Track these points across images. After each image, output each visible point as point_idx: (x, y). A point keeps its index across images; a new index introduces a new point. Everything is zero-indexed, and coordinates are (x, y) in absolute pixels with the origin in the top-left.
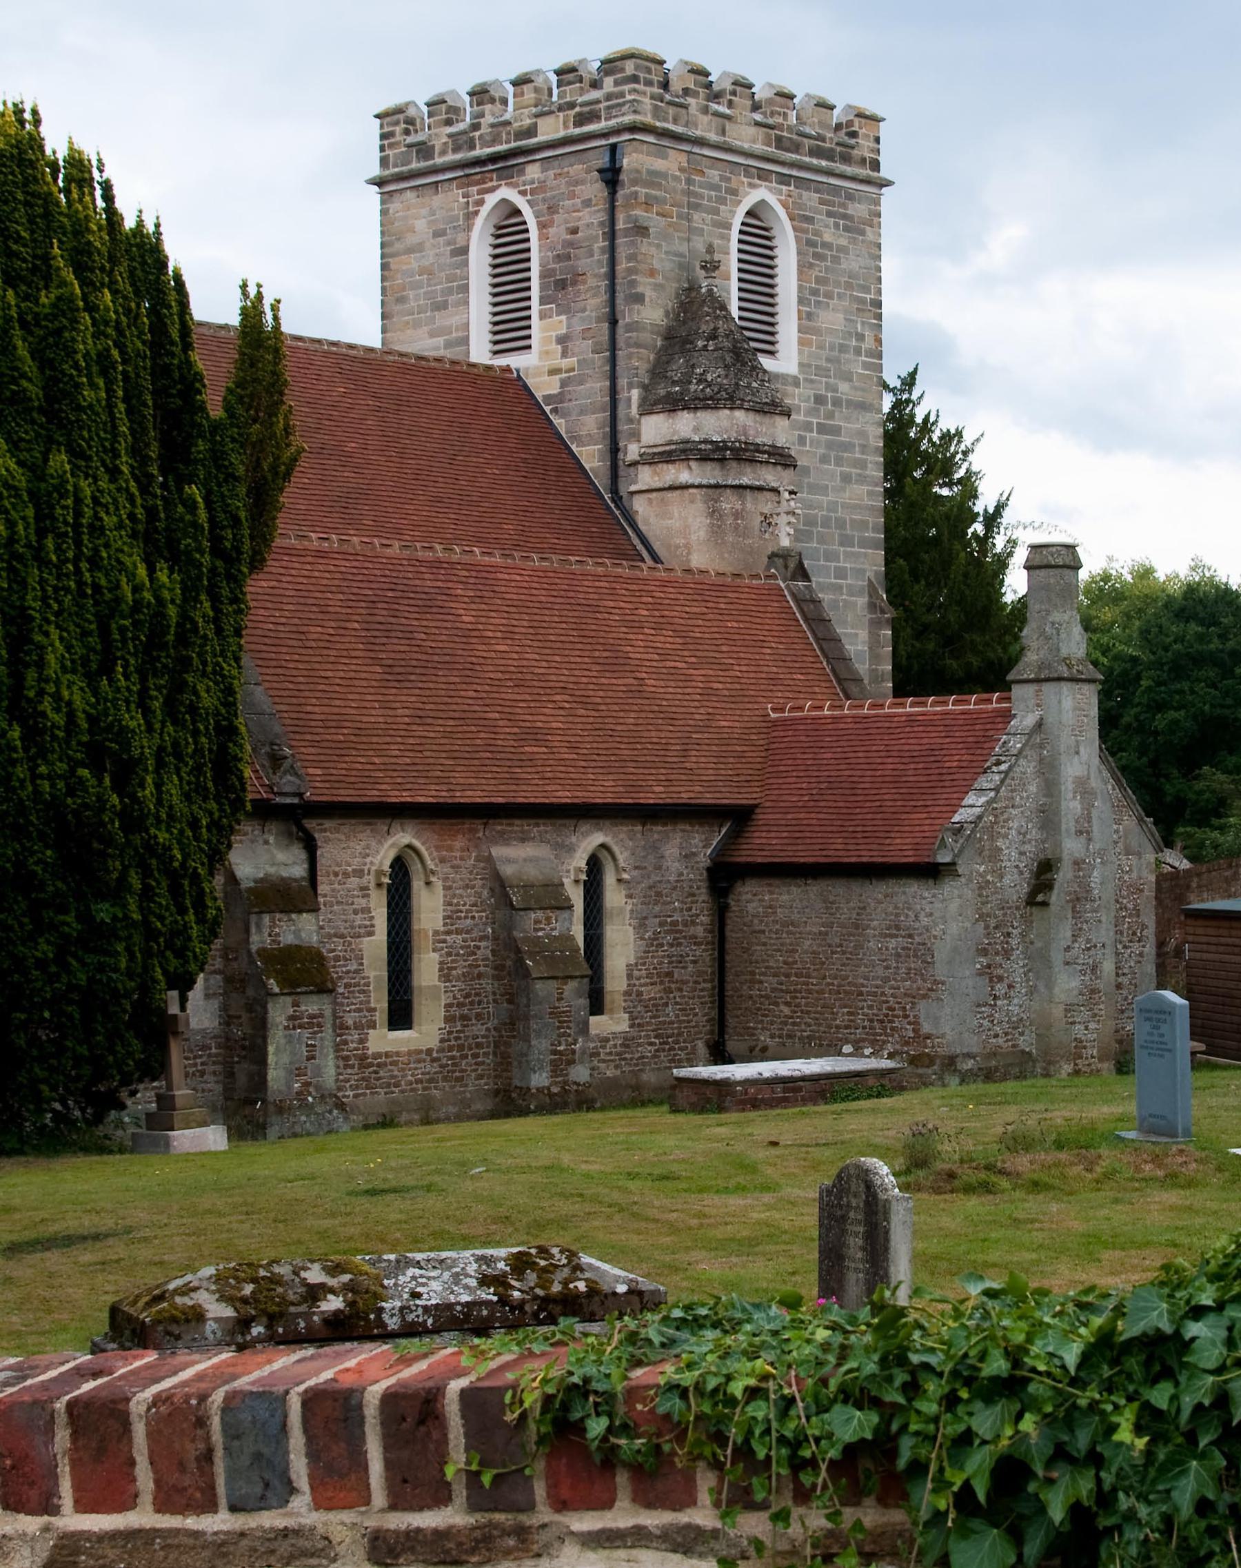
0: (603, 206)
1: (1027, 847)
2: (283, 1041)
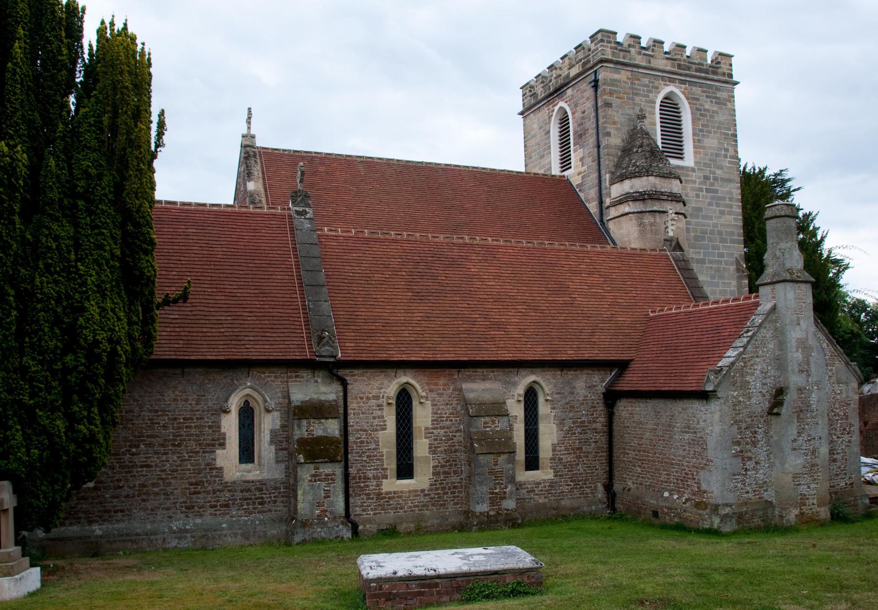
0: (592, 98)
1: (768, 380)
2: (308, 488)
